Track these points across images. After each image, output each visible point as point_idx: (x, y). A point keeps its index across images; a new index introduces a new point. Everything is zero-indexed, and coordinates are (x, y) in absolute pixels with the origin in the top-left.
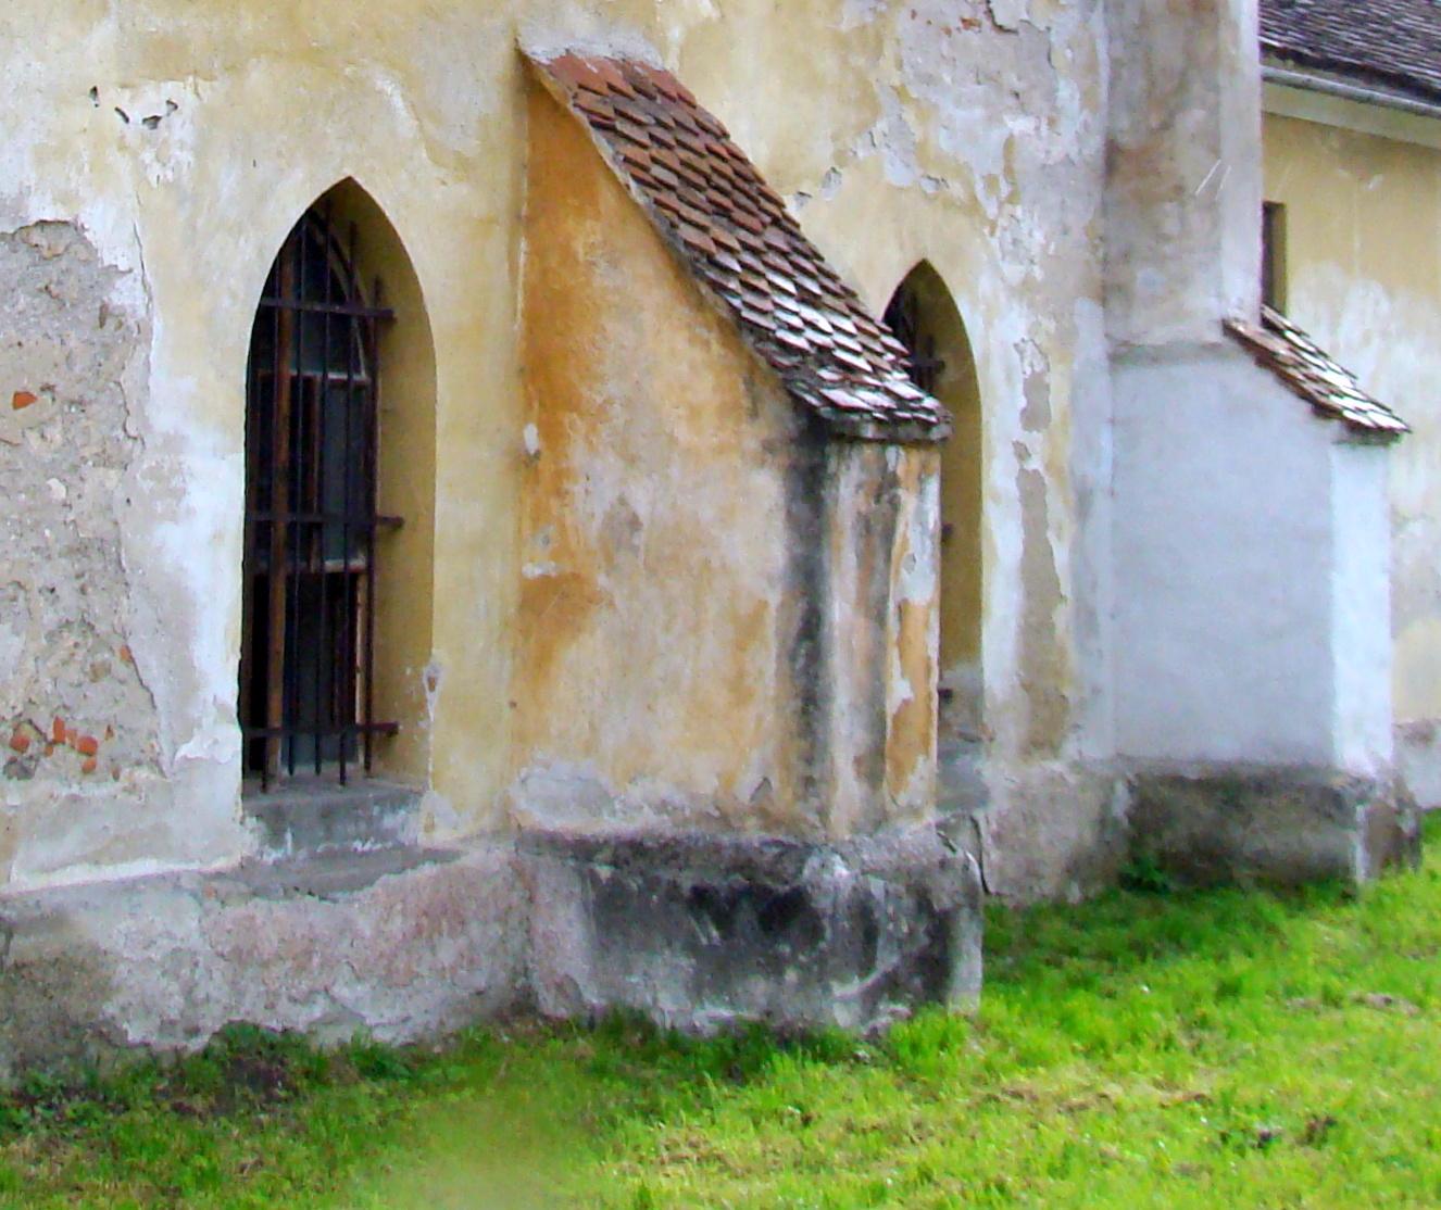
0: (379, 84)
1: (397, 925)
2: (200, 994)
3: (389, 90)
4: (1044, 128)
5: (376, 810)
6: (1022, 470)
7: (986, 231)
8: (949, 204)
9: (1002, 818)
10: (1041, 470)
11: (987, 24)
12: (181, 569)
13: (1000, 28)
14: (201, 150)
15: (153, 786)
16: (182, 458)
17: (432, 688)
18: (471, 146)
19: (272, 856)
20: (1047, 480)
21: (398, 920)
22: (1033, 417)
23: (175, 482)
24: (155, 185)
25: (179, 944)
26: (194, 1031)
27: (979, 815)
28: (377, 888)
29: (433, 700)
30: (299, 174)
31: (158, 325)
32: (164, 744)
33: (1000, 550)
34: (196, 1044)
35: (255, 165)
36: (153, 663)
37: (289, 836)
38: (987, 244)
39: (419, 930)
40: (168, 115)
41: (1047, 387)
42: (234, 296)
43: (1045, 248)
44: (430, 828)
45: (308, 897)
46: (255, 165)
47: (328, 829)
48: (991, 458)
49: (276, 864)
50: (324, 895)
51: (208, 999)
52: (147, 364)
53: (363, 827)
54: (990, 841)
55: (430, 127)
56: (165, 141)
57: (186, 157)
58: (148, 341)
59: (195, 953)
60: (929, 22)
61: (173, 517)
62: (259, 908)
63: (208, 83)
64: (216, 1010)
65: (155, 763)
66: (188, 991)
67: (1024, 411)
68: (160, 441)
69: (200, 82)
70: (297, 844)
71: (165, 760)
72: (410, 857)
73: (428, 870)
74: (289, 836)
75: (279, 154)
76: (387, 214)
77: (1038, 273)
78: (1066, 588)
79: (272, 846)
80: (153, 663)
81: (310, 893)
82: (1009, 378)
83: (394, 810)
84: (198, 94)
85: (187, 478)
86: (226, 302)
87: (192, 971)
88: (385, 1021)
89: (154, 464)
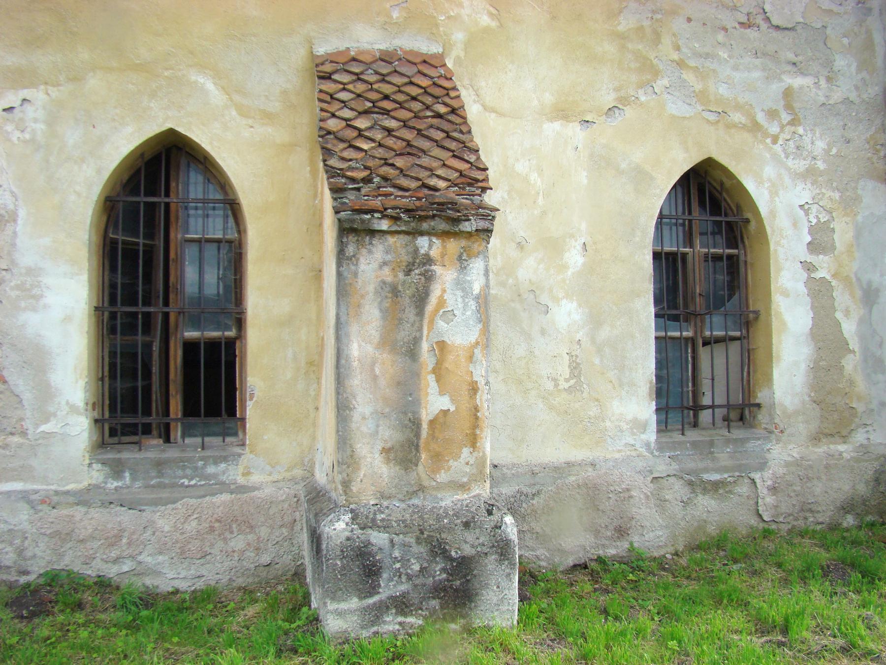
0: (193, 78)
1: (192, 526)
2: (29, 554)
3: (202, 81)
4: (823, 82)
5: (201, 463)
6: (810, 278)
7: (768, 141)
8: (730, 126)
9: (775, 476)
10: (828, 277)
11: (764, 26)
12: (40, 336)
13: (777, 28)
14: (52, 121)
15: (20, 446)
16: (40, 279)
17: (251, 399)
18: (275, 106)
19: (113, 484)
20: (834, 283)
21: (194, 524)
22: (820, 243)
23: (36, 291)
24: (16, 142)
25: (12, 527)
26: (26, 573)
27: (757, 476)
28: (179, 505)
29: (250, 404)
30: (130, 129)
31: (22, 213)
32: (28, 424)
33: (788, 317)
34: (23, 580)
35: (94, 127)
36: (21, 382)
37: (127, 474)
38: (770, 149)
39: (212, 529)
40: (21, 105)
41: (833, 230)
42: (79, 195)
43: (827, 152)
44: (247, 474)
45: (119, 508)
46: (94, 127)
47: (159, 472)
48: (779, 270)
49: (116, 489)
50: (133, 506)
51: (35, 556)
52: (15, 233)
53: (189, 472)
54: (765, 491)
55: (237, 98)
56: (21, 120)
57: (41, 126)
58: (15, 221)
59: (26, 532)
60: (704, 24)
61: (34, 310)
62: (79, 512)
63: (55, 89)
64: (43, 563)
65: (24, 434)
66: (20, 552)
67: (809, 243)
68: (23, 271)
69: (50, 88)
70: (134, 479)
71: (30, 432)
72: (224, 487)
73: (225, 497)
74: (127, 474)
75: (114, 120)
76: (203, 145)
77: (821, 165)
78: (854, 344)
79: (114, 479)
80: (21, 382)
81: (121, 505)
82: (795, 225)
83: (216, 463)
84: (48, 94)
85: (44, 290)
86: (73, 198)
87: (23, 542)
88: (181, 576)
89: (19, 282)
